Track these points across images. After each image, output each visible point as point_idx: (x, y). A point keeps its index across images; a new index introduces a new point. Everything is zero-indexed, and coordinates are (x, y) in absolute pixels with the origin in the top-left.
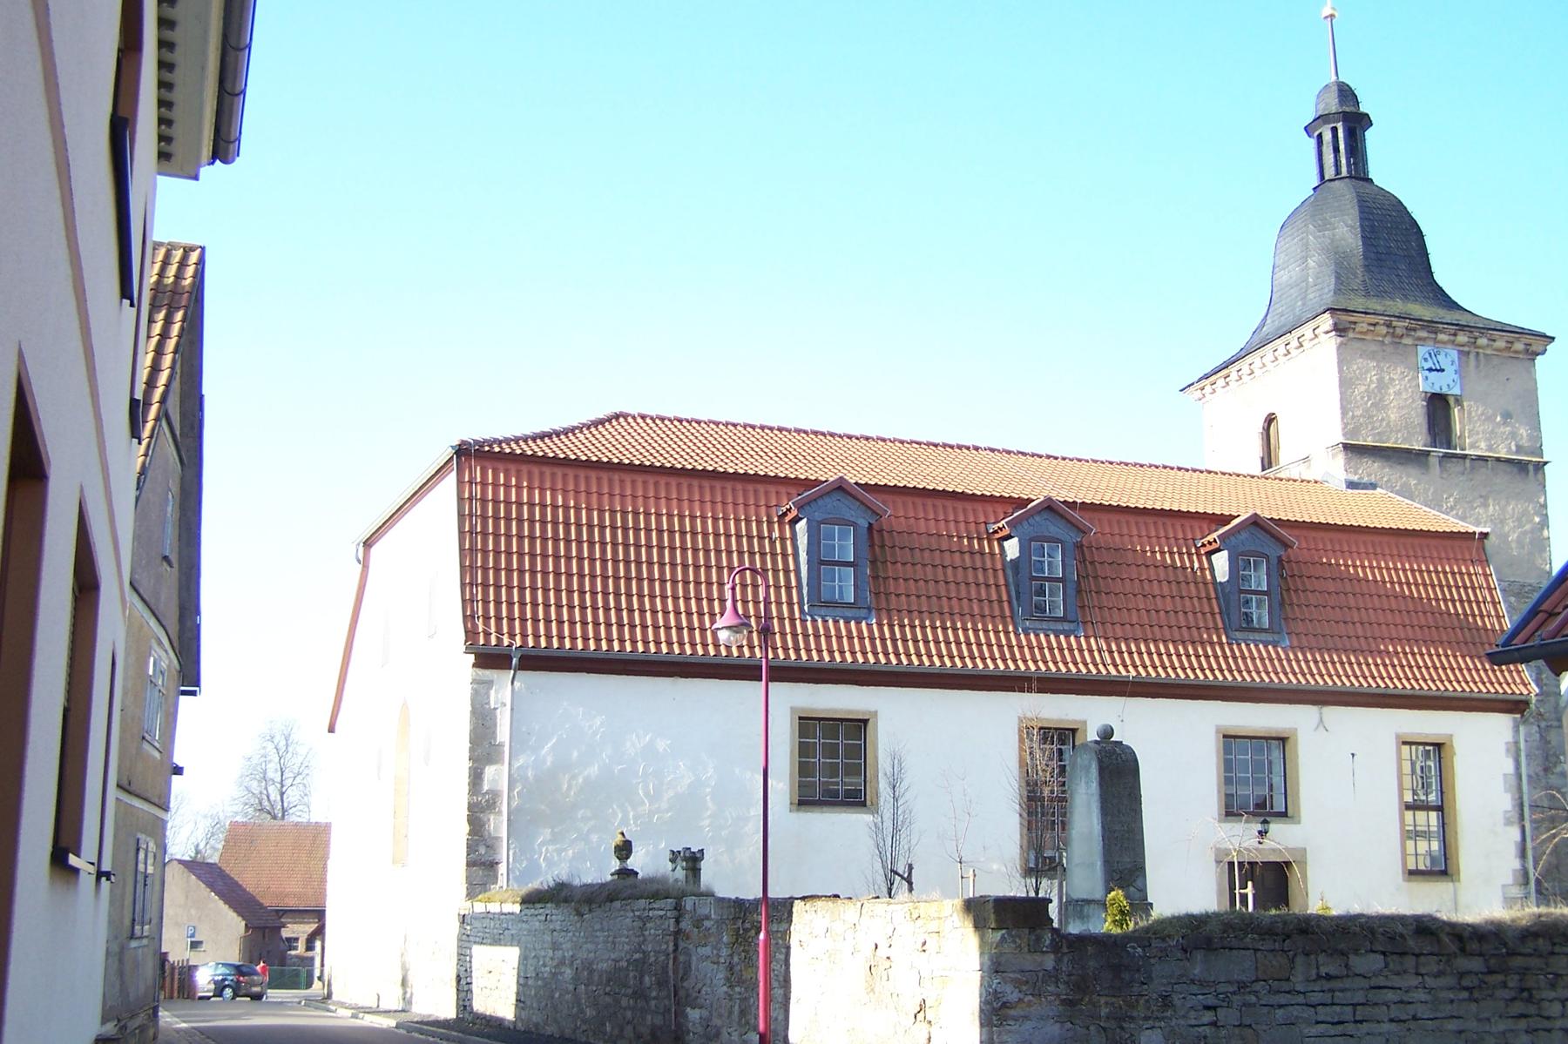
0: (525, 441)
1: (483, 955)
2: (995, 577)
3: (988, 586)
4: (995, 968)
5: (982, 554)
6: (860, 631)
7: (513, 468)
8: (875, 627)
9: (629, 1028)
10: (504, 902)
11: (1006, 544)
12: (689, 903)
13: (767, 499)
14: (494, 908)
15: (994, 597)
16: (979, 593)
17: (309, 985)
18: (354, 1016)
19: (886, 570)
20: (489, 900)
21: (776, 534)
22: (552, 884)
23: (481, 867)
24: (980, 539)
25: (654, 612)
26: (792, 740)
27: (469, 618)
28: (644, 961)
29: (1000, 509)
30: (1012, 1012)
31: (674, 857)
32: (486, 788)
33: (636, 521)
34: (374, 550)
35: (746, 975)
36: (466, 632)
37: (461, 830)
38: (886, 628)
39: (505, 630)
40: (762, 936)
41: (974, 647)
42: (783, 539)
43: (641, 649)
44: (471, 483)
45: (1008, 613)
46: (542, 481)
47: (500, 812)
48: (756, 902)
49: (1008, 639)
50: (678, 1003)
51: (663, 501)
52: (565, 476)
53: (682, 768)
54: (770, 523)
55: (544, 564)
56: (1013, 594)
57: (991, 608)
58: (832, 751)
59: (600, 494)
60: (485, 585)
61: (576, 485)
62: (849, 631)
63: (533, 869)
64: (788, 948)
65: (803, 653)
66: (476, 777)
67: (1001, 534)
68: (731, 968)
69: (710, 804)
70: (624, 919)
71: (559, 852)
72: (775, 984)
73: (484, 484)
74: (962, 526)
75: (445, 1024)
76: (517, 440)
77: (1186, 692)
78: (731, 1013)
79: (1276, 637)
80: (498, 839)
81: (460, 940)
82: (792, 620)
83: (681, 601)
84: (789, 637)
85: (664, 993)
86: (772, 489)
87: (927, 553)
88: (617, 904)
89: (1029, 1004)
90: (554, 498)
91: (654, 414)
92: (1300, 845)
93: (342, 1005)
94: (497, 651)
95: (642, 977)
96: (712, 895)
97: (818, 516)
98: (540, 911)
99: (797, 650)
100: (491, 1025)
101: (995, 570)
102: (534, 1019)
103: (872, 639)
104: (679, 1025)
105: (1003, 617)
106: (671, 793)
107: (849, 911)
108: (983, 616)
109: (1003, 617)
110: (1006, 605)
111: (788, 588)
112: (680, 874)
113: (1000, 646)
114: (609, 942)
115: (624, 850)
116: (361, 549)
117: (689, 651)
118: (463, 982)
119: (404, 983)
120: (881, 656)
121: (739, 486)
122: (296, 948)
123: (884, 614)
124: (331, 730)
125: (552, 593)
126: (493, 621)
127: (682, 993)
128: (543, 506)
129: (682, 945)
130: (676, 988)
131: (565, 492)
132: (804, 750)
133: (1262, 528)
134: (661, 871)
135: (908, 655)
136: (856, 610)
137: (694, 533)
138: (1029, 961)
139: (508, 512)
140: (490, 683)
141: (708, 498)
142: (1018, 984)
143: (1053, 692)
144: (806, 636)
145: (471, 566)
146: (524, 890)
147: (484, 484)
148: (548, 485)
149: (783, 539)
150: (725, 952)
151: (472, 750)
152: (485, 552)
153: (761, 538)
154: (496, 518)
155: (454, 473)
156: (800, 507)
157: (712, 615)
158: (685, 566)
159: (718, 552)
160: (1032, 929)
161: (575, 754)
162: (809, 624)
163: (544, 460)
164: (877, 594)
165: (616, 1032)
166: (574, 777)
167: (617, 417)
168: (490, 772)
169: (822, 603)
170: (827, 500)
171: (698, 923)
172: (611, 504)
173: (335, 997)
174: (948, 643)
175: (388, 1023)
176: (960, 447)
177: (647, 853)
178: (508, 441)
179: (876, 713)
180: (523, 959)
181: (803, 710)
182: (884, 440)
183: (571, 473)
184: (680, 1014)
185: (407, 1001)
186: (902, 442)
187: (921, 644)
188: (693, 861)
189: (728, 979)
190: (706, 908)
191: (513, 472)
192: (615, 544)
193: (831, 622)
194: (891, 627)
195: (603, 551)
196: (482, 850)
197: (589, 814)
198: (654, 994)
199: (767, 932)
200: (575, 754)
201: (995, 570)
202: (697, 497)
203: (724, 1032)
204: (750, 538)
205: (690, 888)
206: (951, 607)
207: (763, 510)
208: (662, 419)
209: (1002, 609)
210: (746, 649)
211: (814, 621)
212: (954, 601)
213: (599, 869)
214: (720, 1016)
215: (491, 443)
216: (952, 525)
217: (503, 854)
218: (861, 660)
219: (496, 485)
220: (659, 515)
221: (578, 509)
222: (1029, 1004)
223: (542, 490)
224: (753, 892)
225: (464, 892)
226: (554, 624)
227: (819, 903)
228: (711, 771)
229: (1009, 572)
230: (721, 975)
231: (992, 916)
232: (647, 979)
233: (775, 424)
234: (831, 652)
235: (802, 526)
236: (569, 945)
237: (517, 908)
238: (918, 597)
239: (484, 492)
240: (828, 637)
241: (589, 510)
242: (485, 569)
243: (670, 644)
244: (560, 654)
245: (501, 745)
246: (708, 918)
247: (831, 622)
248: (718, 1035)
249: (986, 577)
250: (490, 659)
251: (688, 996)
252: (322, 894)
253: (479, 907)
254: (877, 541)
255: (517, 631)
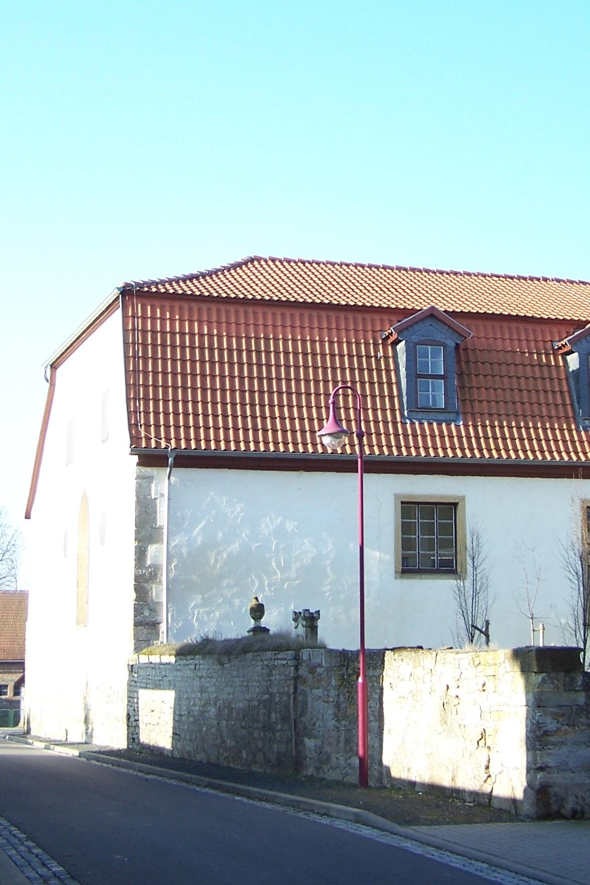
0: (177, 282)
1: (146, 696)
2: (560, 385)
3: (554, 392)
4: (538, 703)
5: (549, 365)
6: (450, 431)
7: (167, 304)
8: (462, 427)
9: (260, 756)
10: (162, 655)
11: (569, 358)
12: (305, 654)
13: (373, 326)
14: (155, 659)
15: (560, 402)
16: (547, 398)
17: (16, 724)
18: (47, 748)
19: (470, 381)
20: (151, 653)
21: (380, 354)
22: (199, 640)
23: (146, 626)
24: (547, 355)
25: (283, 419)
26: (396, 521)
27: (133, 426)
28: (270, 700)
29: (563, 330)
30: (552, 739)
31: (297, 616)
32: (149, 562)
33: (267, 345)
34: (58, 371)
35: (350, 711)
36: (131, 437)
37: (131, 596)
38: (471, 429)
39: (163, 435)
40: (360, 680)
41: (543, 442)
42: (386, 358)
43: (272, 448)
44: (133, 317)
45: (570, 415)
46: (190, 315)
47: (161, 582)
48: (358, 652)
49: (571, 435)
50: (298, 735)
51: (289, 329)
52: (227, 312)
53: (303, 544)
54: (376, 345)
55: (194, 381)
56: (575, 398)
57: (557, 411)
58: (429, 529)
59: (247, 325)
60: (146, 400)
61: (228, 317)
62: (441, 431)
63: (187, 628)
64: (382, 689)
65: (403, 450)
66: (141, 555)
67: (564, 350)
68: (338, 705)
69: (329, 573)
70: (255, 668)
71: (208, 613)
72: (372, 718)
73: (144, 318)
74: (532, 344)
75: (117, 753)
76: (170, 282)
78: (338, 741)
80: (160, 603)
81: (129, 685)
82: (395, 423)
83: (304, 409)
84: (392, 437)
85: (285, 727)
86: (377, 317)
87: (504, 367)
88: (250, 655)
89: (566, 732)
90: (200, 328)
91: (282, 258)
93: (38, 739)
94: (157, 452)
95: (270, 713)
96: (324, 647)
97: (414, 338)
98: (190, 661)
99: (399, 447)
100: (153, 754)
101: (560, 380)
102: (187, 748)
103: (460, 437)
104: (299, 752)
105: (567, 418)
106: (298, 565)
107: (426, 659)
108: (550, 417)
109: (567, 418)
110: (569, 408)
111: (391, 397)
112: (301, 630)
113: (565, 442)
114: (242, 687)
115: (258, 611)
116: (49, 370)
117: (311, 450)
118: (132, 719)
119: (86, 721)
120: (467, 451)
121: (350, 316)
122: (5, 694)
123: (469, 416)
124: (28, 516)
125: (257, 407)
126: (152, 428)
127: (301, 726)
128: (192, 335)
129: (301, 687)
130: (297, 723)
131: (209, 323)
132: (406, 528)
134: (284, 628)
135: (489, 450)
136: (447, 414)
137: (314, 355)
138: (566, 698)
139: (164, 340)
140: (150, 479)
142: (555, 716)
143: (230, 467)
144: (406, 436)
145: (134, 384)
146: (178, 645)
147: (144, 318)
148: (196, 318)
149: (386, 358)
150: (333, 693)
151: (137, 532)
152: (146, 373)
153: (368, 357)
154: (154, 345)
155: (120, 310)
156: (400, 331)
157: (320, 420)
158: (307, 381)
159: (334, 369)
160: (567, 672)
161: (220, 535)
162: (408, 426)
163: (192, 298)
164: (464, 401)
165: (250, 758)
166: (219, 553)
167: (252, 260)
168: (152, 549)
169: (419, 409)
170: (421, 325)
171: (312, 670)
172: (247, 332)
173: (33, 733)
174: (522, 440)
175: (73, 752)
176: (531, 279)
177: (280, 613)
178: (163, 283)
179: (463, 498)
180: (178, 700)
181: (405, 496)
182: (469, 274)
183: (333, 315)
184: (299, 743)
185: (89, 735)
186: (484, 276)
187: (535, 442)
188: (311, 620)
189: (336, 715)
190: (319, 658)
191: (167, 308)
192: (250, 365)
193: (426, 424)
194: (475, 427)
195: (241, 370)
196: (147, 613)
197: (232, 582)
198: (279, 727)
199: (364, 676)
200: (220, 535)
201: (560, 380)
202: (343, 327)
203: (333, 756)
204: (359, 357)
205: (309, 642)
206: (524, 410)
207: (370, 334)
208: (289, 262)
209: (566, 411)
210: (348, 448)
211: (412, 424)
212: (527, 405)
213: (238, 627)
214: (330, 744)
215: (149, 284)
216: (524, 343)
217: (163, 616)
218: (451, 455)
219: (153, 319)
220: (285, 340)
221: (220, 337)
222: (566, 732)
223: (191, 322)
224: (355, 646)
225: (132, 646)
226: (241, 432)
227: (405, 653)
228: (331, 546)
229: (572, 382)
230: (330, 712)
231: (535, 663)
232: (273, 715)
233: (380, 264)
234: (389, 447)
235: (401, 346)
236: (213, 689)
237: (172, 659)
238: (497, 402)
239: (144, 324)
240: (424, 436)
241: (229, 337)
242: (146, 386)
243: (295, 444)
244: (226, 454)
245: (161, 528)
246: (320, 666)
247: (426, 424)
248: (328, 759)
249: (552, 386)
250: (150, 459)
251: (306, 728)
252: (22, 651)
253: (144, 659)
254: (463, 358)
255: (172, 436)
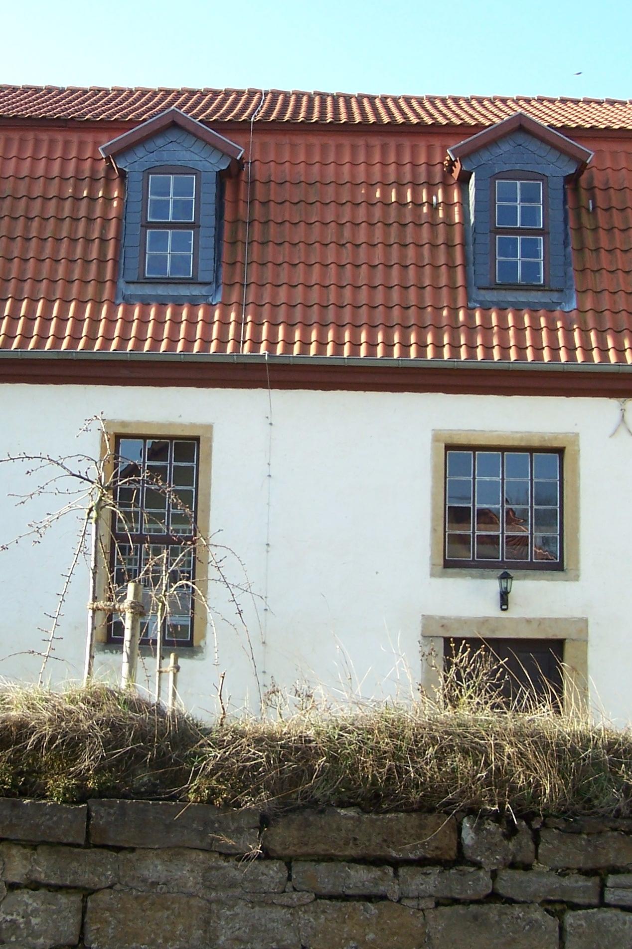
52: (399, 148)
77: (362, 379)
79: (555, 297)
92: (578, 614)
133: (543, 140)
141: (407, 159)
143: (365, 390)
